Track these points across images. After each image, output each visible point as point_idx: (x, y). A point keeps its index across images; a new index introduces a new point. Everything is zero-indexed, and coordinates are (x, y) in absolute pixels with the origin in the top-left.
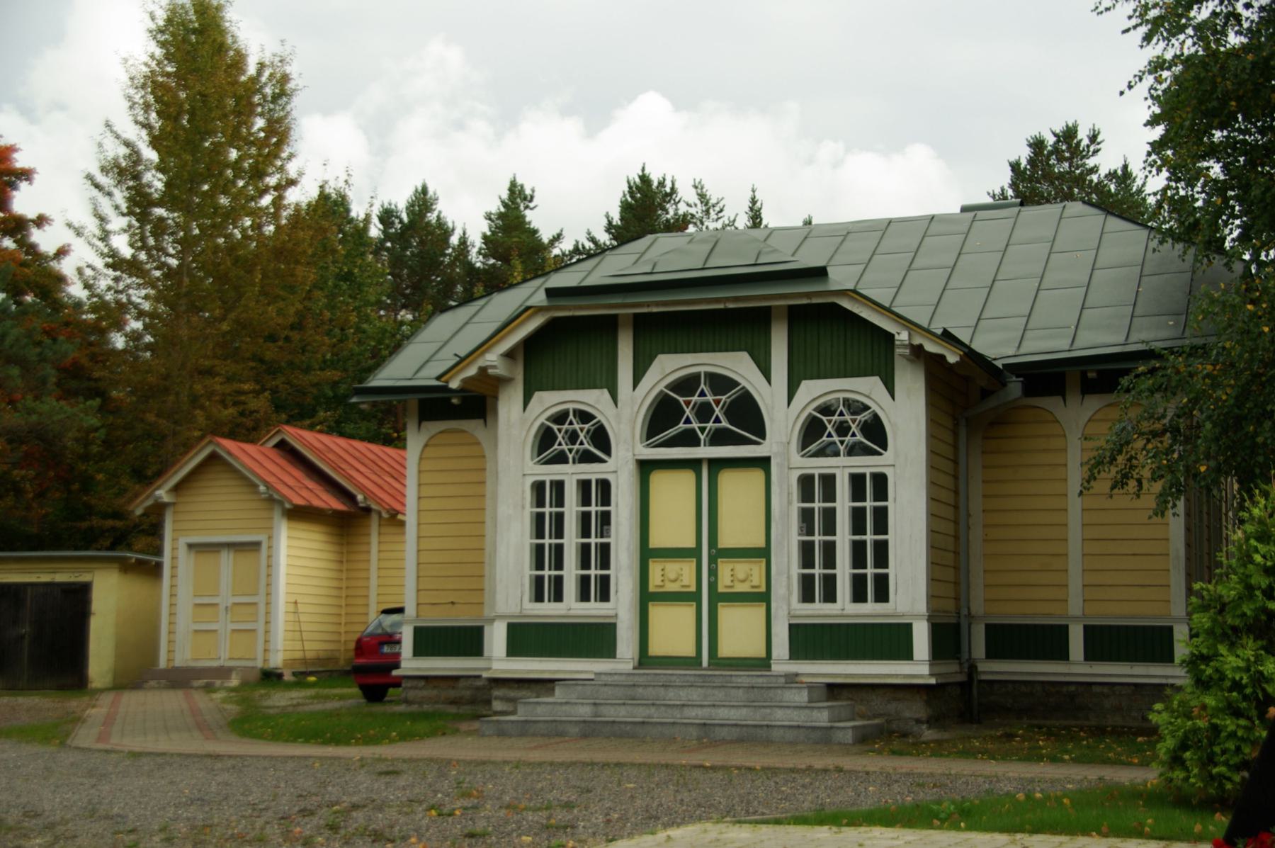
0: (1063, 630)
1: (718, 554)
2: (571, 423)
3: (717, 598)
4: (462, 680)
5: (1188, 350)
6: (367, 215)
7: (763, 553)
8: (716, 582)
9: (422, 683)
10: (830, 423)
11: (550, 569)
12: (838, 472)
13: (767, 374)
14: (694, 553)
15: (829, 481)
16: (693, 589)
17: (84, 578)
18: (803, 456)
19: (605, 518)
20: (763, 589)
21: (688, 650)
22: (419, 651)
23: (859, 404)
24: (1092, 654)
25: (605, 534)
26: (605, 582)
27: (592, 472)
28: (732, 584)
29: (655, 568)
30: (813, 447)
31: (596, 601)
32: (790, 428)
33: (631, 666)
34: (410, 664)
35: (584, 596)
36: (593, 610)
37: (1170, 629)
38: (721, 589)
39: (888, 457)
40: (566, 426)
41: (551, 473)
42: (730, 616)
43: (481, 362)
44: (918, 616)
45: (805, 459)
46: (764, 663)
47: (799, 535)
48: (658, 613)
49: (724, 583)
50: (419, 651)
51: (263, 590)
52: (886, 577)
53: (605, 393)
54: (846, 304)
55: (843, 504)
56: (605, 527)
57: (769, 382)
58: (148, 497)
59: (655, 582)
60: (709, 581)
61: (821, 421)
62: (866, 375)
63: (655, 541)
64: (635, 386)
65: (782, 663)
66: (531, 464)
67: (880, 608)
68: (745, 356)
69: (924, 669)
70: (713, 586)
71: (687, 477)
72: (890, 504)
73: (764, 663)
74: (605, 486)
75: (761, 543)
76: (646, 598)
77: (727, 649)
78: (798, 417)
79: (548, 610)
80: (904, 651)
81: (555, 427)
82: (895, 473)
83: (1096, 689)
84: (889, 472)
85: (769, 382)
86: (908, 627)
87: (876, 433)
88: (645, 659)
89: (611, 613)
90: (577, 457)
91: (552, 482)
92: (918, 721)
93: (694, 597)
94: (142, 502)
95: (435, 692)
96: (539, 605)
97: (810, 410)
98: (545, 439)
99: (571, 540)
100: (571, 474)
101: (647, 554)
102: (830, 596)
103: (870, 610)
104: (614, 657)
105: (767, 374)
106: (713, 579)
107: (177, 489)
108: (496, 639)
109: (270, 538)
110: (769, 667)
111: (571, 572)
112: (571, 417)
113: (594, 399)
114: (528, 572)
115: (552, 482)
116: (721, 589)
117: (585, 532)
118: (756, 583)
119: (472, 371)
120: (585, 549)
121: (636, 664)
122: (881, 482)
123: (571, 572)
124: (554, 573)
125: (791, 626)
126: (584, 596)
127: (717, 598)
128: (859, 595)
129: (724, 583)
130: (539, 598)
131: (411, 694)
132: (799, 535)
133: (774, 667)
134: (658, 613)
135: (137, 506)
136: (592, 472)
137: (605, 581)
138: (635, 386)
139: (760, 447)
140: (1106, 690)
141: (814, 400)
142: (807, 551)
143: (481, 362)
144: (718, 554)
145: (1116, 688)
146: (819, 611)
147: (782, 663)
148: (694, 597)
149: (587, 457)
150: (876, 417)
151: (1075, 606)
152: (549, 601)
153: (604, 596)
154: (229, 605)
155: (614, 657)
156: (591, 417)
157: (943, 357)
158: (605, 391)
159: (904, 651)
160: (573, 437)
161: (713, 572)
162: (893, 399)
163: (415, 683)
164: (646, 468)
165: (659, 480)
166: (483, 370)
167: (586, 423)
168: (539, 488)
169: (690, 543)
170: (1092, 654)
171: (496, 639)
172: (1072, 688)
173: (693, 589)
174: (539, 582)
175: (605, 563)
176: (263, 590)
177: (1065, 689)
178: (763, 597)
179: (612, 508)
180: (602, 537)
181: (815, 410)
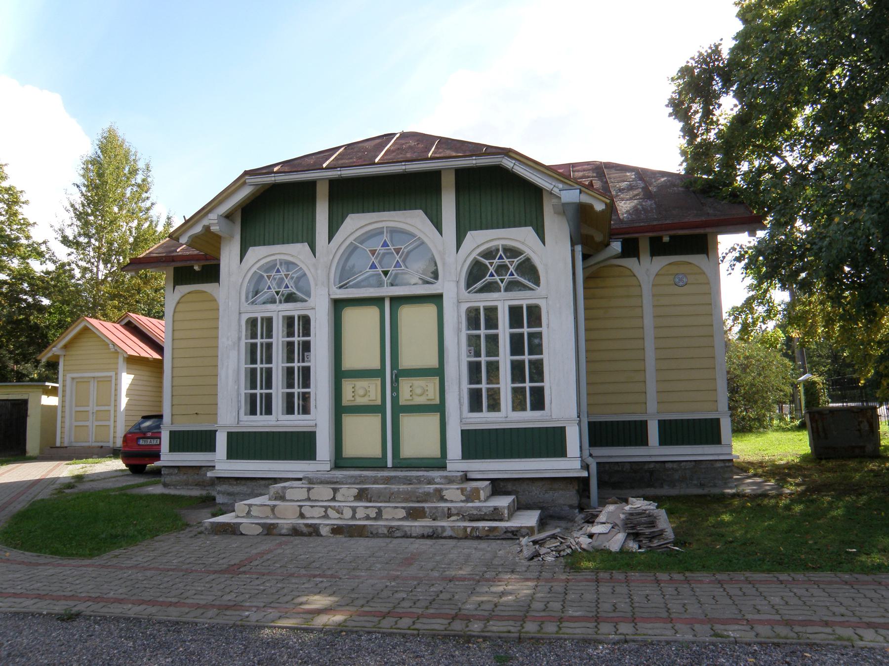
0: (643, 425)
1: (400, 374)
2: (501, 257)
3: (399, 409)
4: (204, 469)
7: (438, 372)
8: (398, 396)
9: (176, 471)
10: (492, 265)
11: (261, 388)
12: (499, 305)
13: (438, 226)
14: (379, 373)
15: (491, 313)
16: (379, 402)
17: (24, 397)
18: (469, 292)
19: (306, 347)
20: (437, 401)
21: (376, 452)
22: (173, 448)
23: (631, 175)
24: (665, 440)
25: (306, 359)
28: (411, 398)
29: (348, 386)
30: (479, 285)
31: (299, 413)
32: (459, 268)
33: (328, 467)
34: (168, 458)
35: (290, 410)
36: (296, 422)
37: (718, 420)
38: (402, 402)
39: (541, 290)
41: (260, 312)
42: (408, 422)
43: (205, 222)
44: (569, 420)
45: (471, 295)
46: (440, 464)
47: (468, 356)
48: (349, 421)
49: (405, 397)
50: (173, 448)
51: (113, 404)
52: (541, 390)
53: (305, 247)
54: (508, 163)
55: (504, 331)
56: (306, 354)
57: (441, 234)
58: (49, 351)
59: (347, 398)
60: (392, 396)
62: (520, 226)
63: (349, 363)
64: (330, 239)
65: (456, 463)
66: (246, 304)
67: (537, 414)
68: (420, 213)
69: (577, 464)
70: (395, 400)
71: (373, 312)
72: (544, 329)
73: (440, 464)
74: (306, 321)
75: (433, 362)
76: (340, 410)
77: (408, 451)
78: (465, 261)
79: (260, 423)
80: (560, 451)
82: (547, 304)
83: (668, 465)
84: (542, 303)
85: (441, 234)
86: (562, 430)
88: (340, 462)
89: (312, 423)
90: (283, 299)
91: (262, 319)
92: (571, 507)
93: (379, 409)
94: (46, 354)
95: (185, 477)
96: (253, 417)
97: (474, 255)
99: (278, 365)
100: (502, 301)
101: (339, 375)
102: (494, 406)
103: (529, 418)
104: (315, 459)
105: (438, 226)
106: (395, 394)
107: (66, 347)
109: (116, 374)
110: (444, 467)
111: (278, 391)
113: (297, 251)
114: (244, 391)
115: (262, 319)
116: (402, 402)
117: (290, 358)
118: (431, 396)
119: (198, 229)
120: (290, 372)
121: (333, 466)
122: (535, 314)
123: (278, 391)
124: (264, 391)
125: (462, 431)
126: (290, 410)
127: (399, 409)
128: (518, 404)
129: (405, 397)
130: (253, 412)
131: (168, 479)
132: (468, 356)
133: (450, 466)
134: (349, 421)
135: (43, 357)
137: (306, 397)
138: (330, 239)
139: (434, 285)
140: (675, 466)
141: (478, 246)
142: (474, 370)
143: (205, 222)
144: (400, 374)
145: (683, 464)
146: (486, 420)
147: (456, 463)
148: (379, 409)
150: (528, 260)
151: (652, 406)
152: (261, 414)
153: (306, 410)
154: (94, 411)
155: (315, 459)
157: (591, 207)
158: (306, 244)
159: (560, 451)
161: (395, 389)
162: (544, 244)
163: (171, 470)
164: (339, 305)
165: (350, 315)
166: (207, 229)
168: (253, 322)
169: (376, 364)
170: (665, 440)
172: (652, 466)
173: (379, 402)
174: (253, 398)
175: (306, 383)
176: (113, 404)
177: (646, 467)
178: (440, 408)
180: (303, 361)
181: (478, 255)
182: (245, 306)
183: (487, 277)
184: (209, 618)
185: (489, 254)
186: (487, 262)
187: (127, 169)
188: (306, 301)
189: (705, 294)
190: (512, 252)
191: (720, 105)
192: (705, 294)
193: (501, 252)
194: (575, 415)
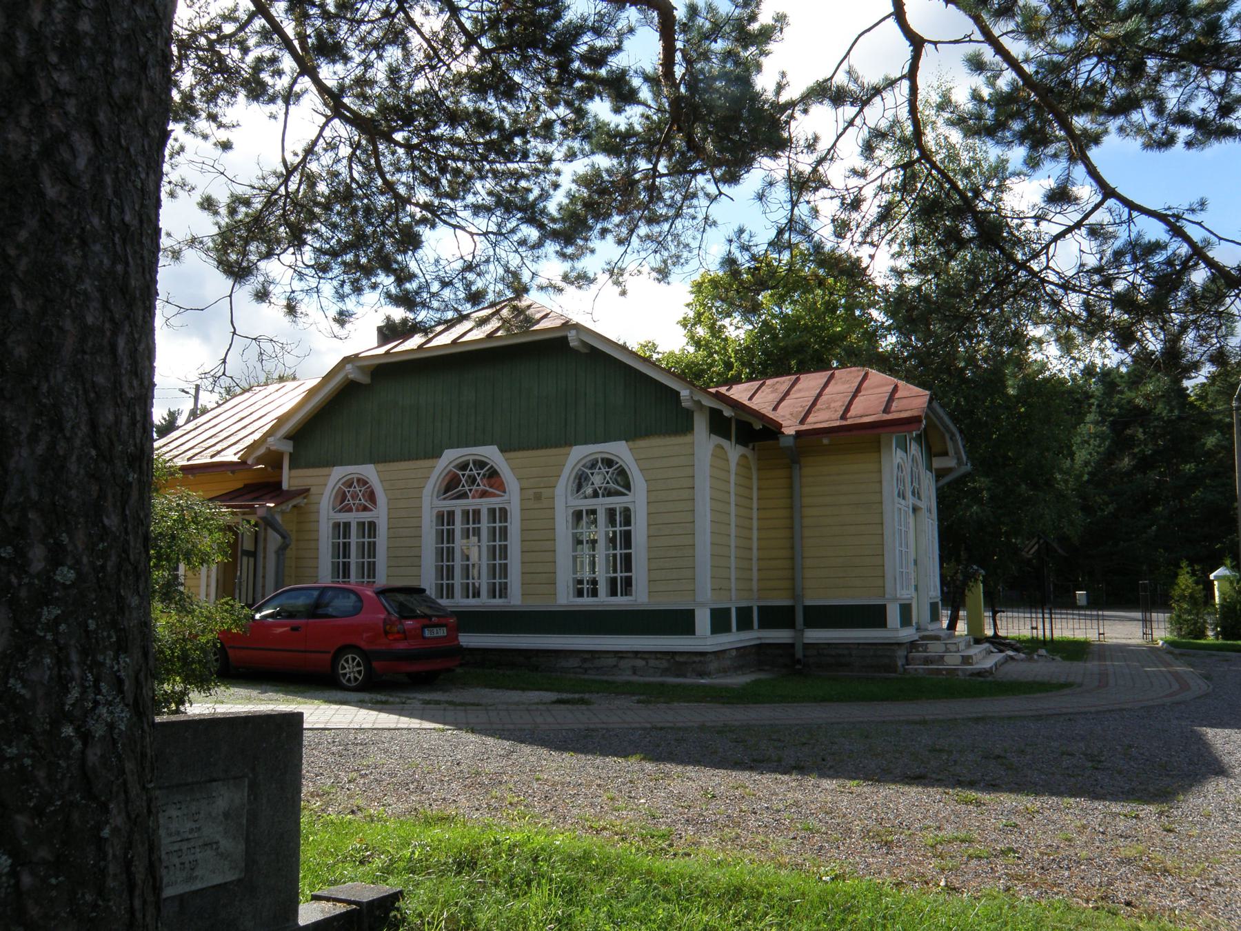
0: (691, 613)
2: (471, 470)
5: (288, 447)
6: (1076, 199)
10: (463, 476)
26: (628, 582)
27: (365, 516)
35: (613, 593)
37: (884, 607)
40: (467, 472)
41: (343, 517)
61: (458, 475)
67: (595, 599)
81: (460, 473)
84: (631, 507)
87: (624, 481)
96: (613, 598)
98: (581, 481)
100: (353, 518)
103: (620, 602)
108: (703, 620)
112: (471, 465)
136: (617, 502)
149: (365, 509)
156: (485, 464)
160: (473, 480)
167: (482, 469)
171: (703, 620)
179: (632, 528)
182: (332, 513)
183: (460, 488)
184: (1093, 709)
185: (464, 466)
186: (589, 472)
187: (90, 344)
188: (371, 510)
189: (764, 509)
190: (480, 464)
191: (879, 206)
192: (764, 509)
193: (471, 465)
194: (813, 599)
